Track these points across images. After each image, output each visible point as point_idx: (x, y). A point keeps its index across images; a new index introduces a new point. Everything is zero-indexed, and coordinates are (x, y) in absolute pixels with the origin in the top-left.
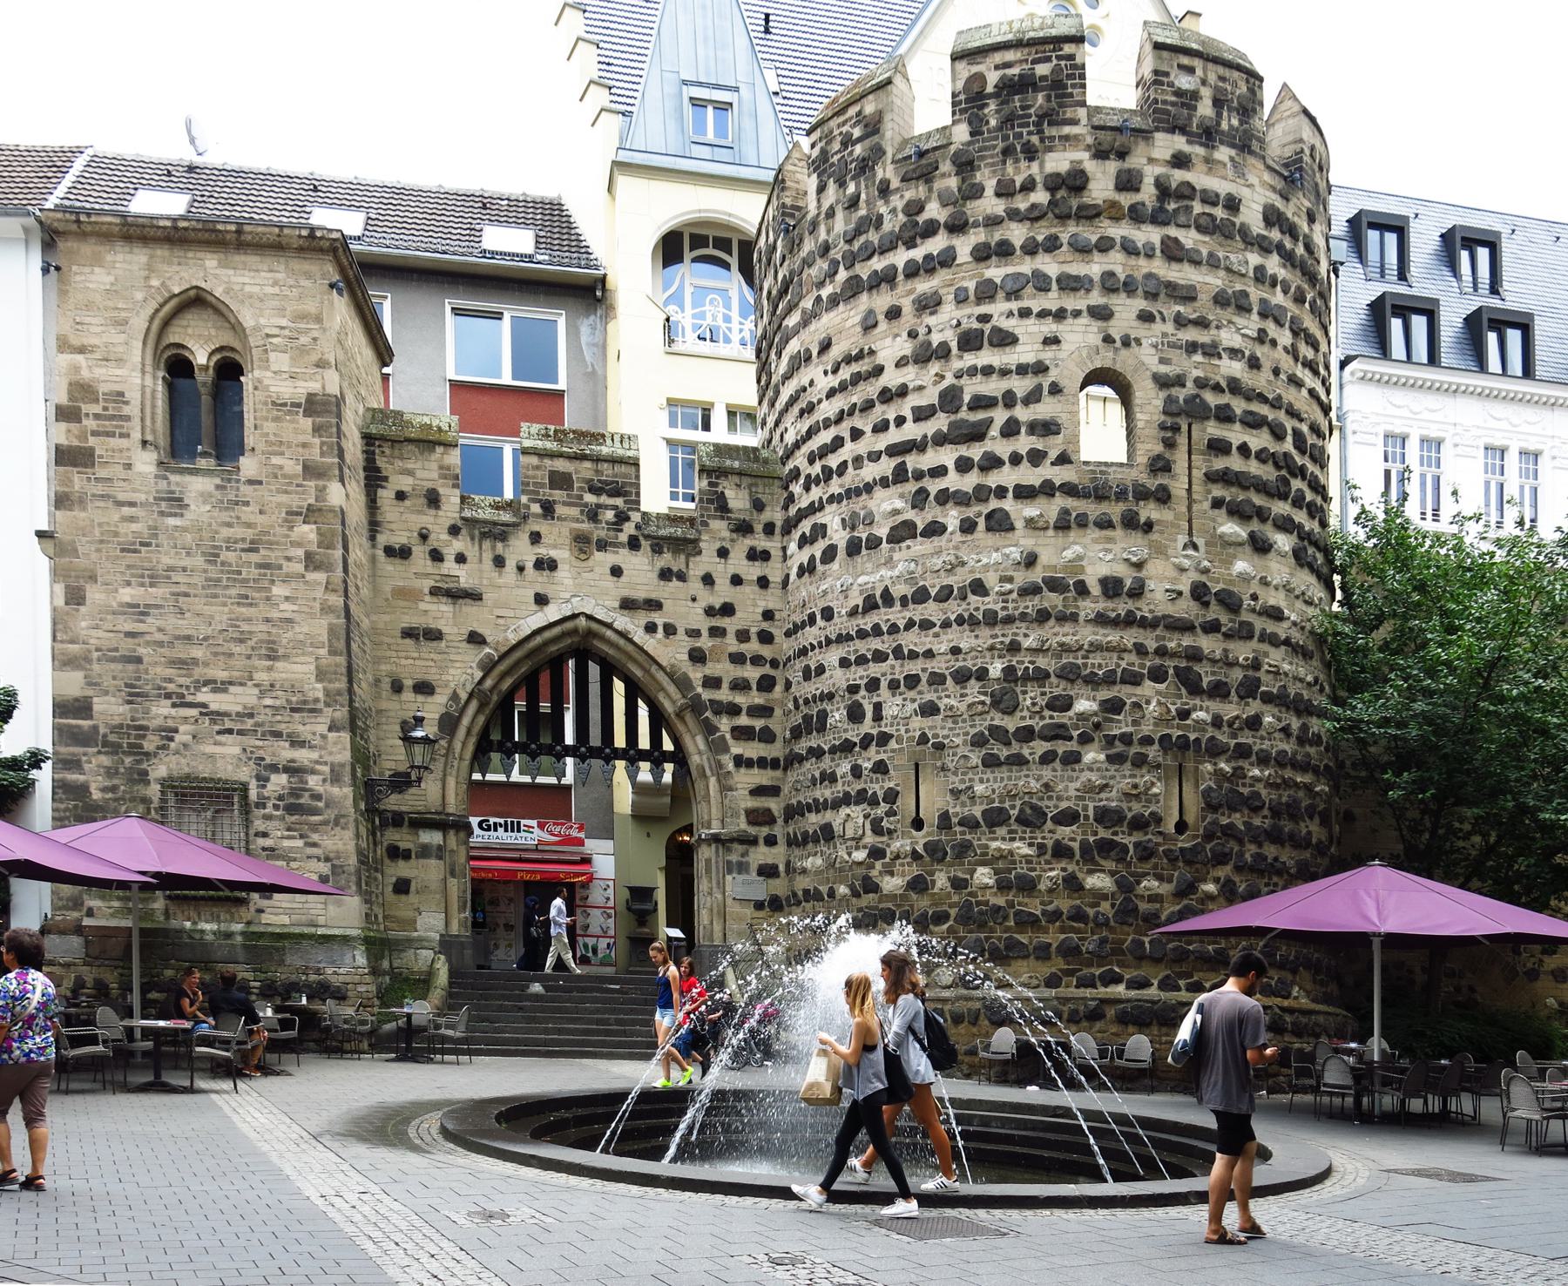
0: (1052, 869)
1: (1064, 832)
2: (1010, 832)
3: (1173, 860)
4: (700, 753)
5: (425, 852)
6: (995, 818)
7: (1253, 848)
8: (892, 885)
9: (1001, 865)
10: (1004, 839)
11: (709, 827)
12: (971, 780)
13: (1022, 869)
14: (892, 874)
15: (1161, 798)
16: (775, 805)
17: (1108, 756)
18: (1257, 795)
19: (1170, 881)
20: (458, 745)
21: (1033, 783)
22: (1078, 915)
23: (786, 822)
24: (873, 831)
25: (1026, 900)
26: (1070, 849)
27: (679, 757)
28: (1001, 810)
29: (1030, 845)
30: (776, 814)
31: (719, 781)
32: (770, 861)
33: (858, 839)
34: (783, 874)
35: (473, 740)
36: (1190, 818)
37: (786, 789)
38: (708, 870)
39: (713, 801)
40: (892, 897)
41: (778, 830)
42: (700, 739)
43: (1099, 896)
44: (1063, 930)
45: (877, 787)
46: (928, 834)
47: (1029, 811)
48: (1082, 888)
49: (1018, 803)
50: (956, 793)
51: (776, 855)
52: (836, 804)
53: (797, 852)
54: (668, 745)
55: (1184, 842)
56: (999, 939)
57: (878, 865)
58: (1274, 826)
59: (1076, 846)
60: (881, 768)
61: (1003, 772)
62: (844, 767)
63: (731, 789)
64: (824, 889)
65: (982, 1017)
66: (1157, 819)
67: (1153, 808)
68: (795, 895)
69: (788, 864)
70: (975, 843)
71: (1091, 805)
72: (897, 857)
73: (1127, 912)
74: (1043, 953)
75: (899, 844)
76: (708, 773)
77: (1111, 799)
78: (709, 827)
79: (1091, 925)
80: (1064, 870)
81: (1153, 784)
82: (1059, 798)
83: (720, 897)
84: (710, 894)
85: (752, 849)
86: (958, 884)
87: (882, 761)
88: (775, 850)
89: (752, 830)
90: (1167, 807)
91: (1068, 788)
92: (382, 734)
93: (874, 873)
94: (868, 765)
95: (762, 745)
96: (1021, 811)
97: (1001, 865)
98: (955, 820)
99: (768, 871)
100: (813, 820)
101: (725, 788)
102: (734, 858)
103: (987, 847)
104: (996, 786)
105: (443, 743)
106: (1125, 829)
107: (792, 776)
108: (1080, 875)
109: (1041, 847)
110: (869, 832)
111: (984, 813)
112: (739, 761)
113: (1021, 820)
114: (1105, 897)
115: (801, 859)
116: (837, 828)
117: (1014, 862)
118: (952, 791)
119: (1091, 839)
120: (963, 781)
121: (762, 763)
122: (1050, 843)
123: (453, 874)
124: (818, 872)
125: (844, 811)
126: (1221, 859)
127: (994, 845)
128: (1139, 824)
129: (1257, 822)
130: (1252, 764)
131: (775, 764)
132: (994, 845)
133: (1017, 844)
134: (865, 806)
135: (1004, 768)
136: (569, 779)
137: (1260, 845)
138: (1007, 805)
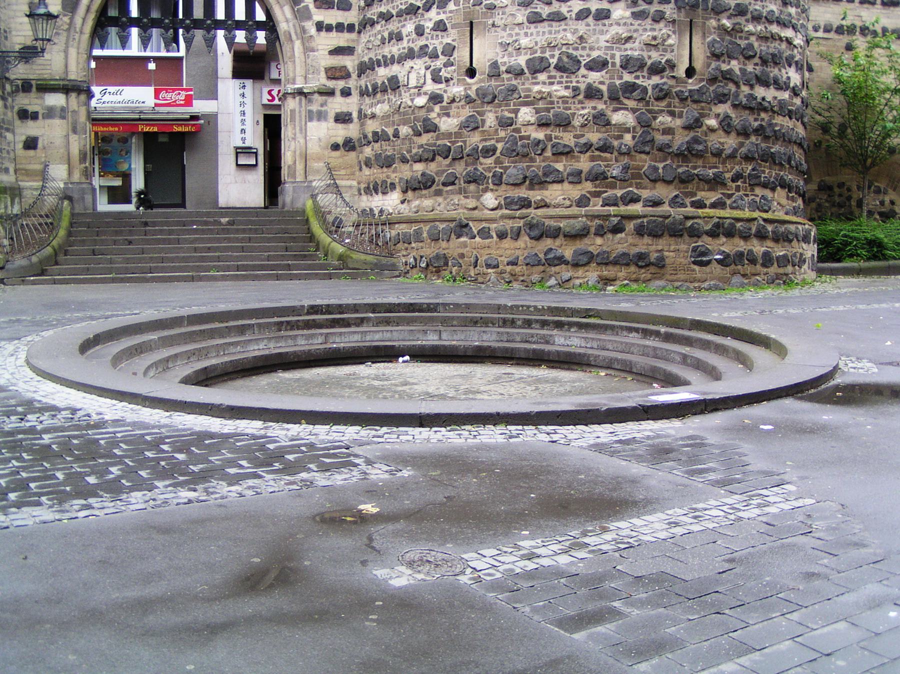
0: (583, 108)
1: (594, 77)
2: (550, 77)
3: (683, 100)
4: (287, 21)
5: (50, 113)
6: (537, 66)
7: (745, 89)
8: (448, 124)
9: (541, 105)
10: (544, 83)
11: (294, 83)
12: (517, 34)
13: (559, 108)
14: (448, 115)
15: (675, 48)
16: (350, 63)
17: (633, 13)
18: (750, 46)
19: (680, 116)
20: (78, 20)
21: (569, 36)
22: (605, 148)
23: (359, 76)
24: (433, 80)
25: (561, 134)
26: (599, 90)
27: (270, 25)
28: (542, 59)
29: (567, 88)
30: (351, 70)
31: (303, 44)
32: (345, 110)
33: (419, 88)
34: (356, 120)
35: (92, 16)
36: (698, 65)
37: (359, 49)
38: (293, 119)
39: (297, 60)
40: (449, 135)
41: (352, 83)
42: (287, 9)
43: (623, 129)
44: (593, 159)
45: (437, 43)
46: (481, 81)
47: (565, 59)
48: (608, 123)
49: (557, 53)
50: (505, 46)
51: (351, 105)
52: (401, 60)
53: (367, 100)
54: (260, 16)
55: (692, 84)
56: (538, 167)
57: (437, 109)
58: (763, 72)
59: (604, 88)
60: (440, 27)
61: (544, 27)
62: (409, 27)
63: (313, 50)
64: (390, 131)
65: (523, 232)
66: (672, 66)
67: (668, 56)
68: (365, 137)
69: (360, 111)
70: (520, 87)
71: (618, 54)
72: (453, 101)
73: (645, 144)
74: (576, 177)
75: (456, 90)
76: (294, 37)
77: (634, 50)
78: (294, 83)
79: (616, 153)
80: (594, 108)
81: (669, 36)
82: (591, 49)
83: (302, 141)
84: (294, 139)
85: (330, 99)
86: (505, 123)
87: (441, 21)
88: (349, 100)
89: (331, 84)
90: (680, 56)
91: (600, 41)
92: (12, 13)
93: (433, 115)
94: (430, 25)
95: (341, 12)
96: (560, 59)
97: (541, 105)
98: (503, 69)
99: (343, 118)
100: (383, 73)
101: (308, 50)
102: (314, 108)
103: (529, 90)
104: (538, 39)
105: (66, 19)
106: (645, 74)
107: (364, 38)
108: (609, 113)
109: (575, 89)
110: (429, 80)
111: (528, 62)
112: (320, 26)
113: (560, 68)
114: (628, 130)
115: (371, 106)
116: (402, 79)
117: (552, 103)
118: (501, 44)
119: (618, 82)
120: (511, 35)
121: (340, 27)
122: (583, 87)
123: (75, 131)
124: (386, 117)
125: (409, 63)
126: (721, 98)
127: (536, 88)
128: (656, 70)
129: (750, 68)
130: (747, 21)
131: (351, 28)
132: (536, 88)
133: (555, 87)
134: (427, 59)
135: (546, 24)
136: (182, 53)
137: (752, 87)
138: (547, 55)
